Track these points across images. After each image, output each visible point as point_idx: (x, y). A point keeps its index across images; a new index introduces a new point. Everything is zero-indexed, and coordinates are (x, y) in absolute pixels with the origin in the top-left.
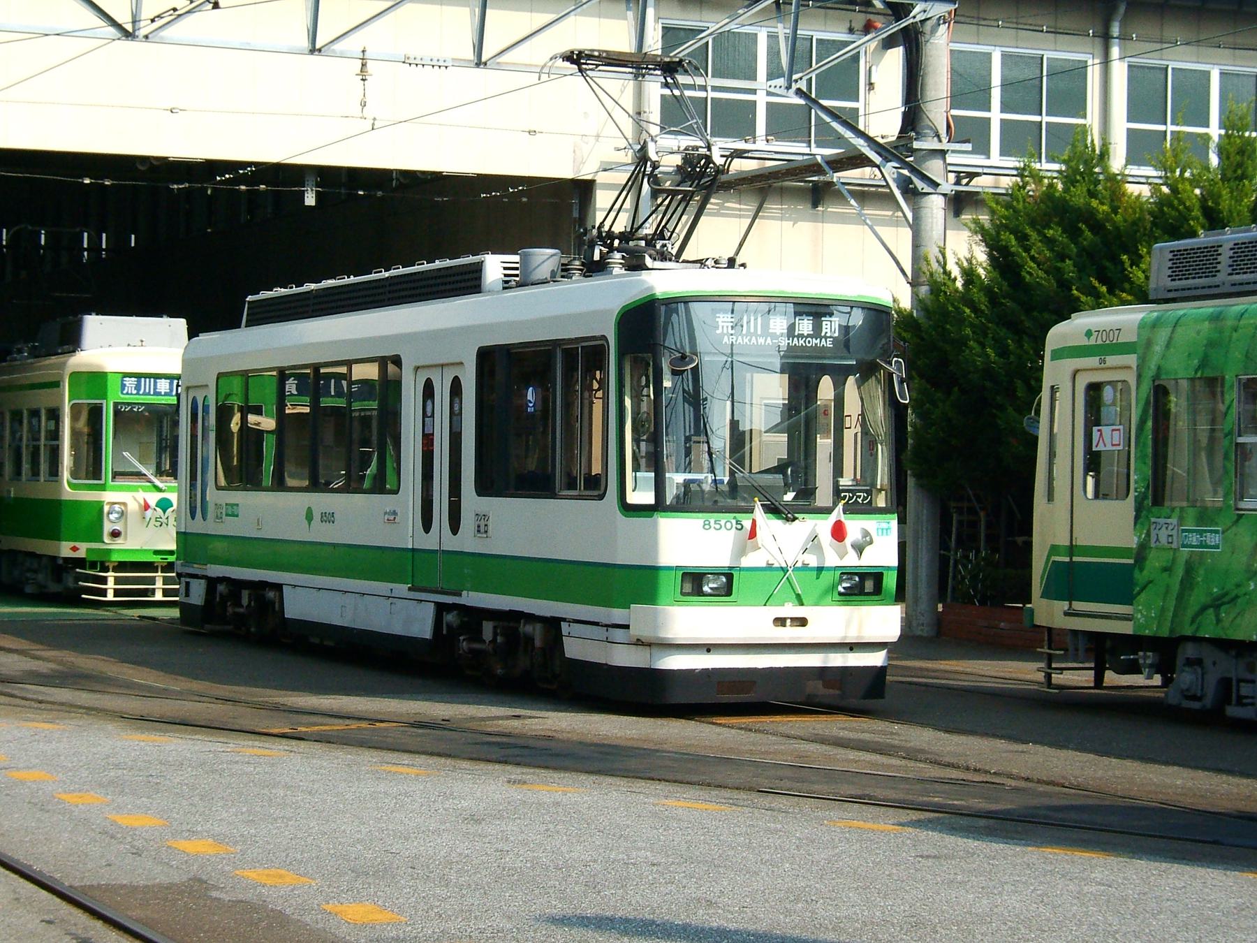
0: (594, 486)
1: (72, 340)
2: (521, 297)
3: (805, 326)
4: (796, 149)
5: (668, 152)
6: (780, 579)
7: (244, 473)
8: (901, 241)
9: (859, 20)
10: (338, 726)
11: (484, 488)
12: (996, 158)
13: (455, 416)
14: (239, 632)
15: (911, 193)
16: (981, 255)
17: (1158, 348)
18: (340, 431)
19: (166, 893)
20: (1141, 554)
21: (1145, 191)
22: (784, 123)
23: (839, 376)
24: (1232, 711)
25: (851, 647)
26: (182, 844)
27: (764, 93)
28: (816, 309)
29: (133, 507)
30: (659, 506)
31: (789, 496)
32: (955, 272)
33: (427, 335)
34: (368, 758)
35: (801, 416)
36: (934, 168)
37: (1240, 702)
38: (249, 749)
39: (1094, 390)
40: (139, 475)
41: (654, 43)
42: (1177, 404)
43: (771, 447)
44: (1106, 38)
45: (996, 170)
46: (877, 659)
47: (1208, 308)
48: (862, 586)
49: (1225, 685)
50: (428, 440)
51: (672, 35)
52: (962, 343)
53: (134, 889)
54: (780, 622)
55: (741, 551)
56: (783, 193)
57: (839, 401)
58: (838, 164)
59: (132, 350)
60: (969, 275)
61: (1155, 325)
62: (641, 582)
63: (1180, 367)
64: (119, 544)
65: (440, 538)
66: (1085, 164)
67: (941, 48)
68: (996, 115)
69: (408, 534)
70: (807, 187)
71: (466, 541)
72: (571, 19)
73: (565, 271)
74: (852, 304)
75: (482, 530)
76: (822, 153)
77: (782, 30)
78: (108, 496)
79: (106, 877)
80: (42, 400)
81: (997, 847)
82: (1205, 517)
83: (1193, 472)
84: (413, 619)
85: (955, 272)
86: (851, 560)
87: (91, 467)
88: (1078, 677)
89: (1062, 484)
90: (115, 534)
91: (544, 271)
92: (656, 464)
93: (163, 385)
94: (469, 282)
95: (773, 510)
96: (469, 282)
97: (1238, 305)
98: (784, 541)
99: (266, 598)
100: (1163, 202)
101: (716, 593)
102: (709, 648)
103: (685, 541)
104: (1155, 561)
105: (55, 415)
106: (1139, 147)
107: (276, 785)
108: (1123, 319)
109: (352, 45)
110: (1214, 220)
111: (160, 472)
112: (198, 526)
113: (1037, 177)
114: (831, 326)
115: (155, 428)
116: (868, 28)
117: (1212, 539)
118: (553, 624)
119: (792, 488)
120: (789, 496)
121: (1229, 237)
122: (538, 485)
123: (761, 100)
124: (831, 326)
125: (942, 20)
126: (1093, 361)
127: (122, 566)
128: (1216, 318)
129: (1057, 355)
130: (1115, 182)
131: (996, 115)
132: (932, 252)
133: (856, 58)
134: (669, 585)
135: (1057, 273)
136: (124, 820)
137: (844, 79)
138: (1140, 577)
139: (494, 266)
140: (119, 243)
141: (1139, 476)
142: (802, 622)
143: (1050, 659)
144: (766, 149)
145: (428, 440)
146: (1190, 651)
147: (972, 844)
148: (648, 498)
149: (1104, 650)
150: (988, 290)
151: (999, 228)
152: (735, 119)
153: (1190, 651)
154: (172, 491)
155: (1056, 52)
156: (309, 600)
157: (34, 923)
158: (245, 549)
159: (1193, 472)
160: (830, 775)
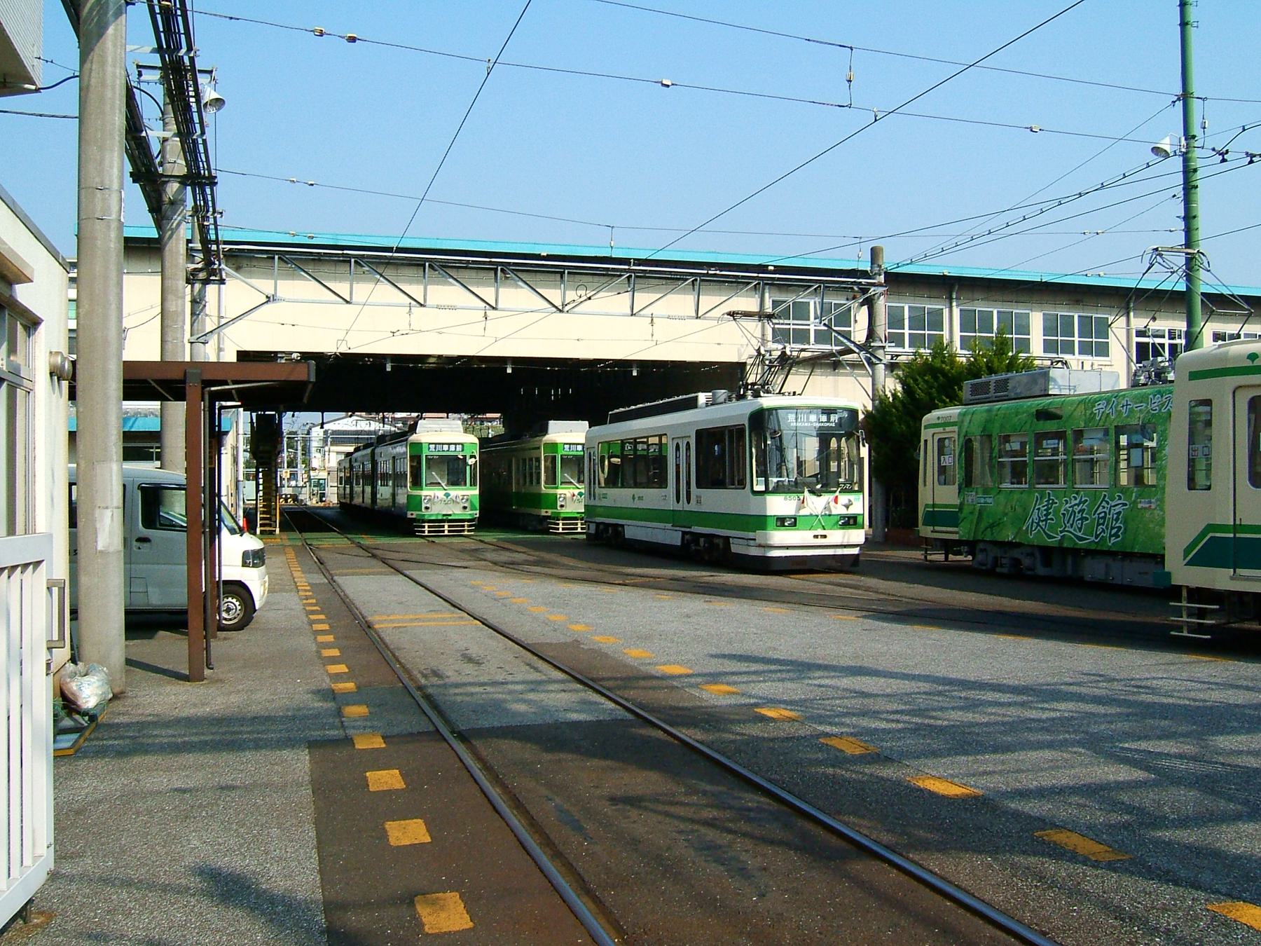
0: (741, 484)
1: (545, 431)
2: (711, 409)
3: (824, 418)
4: (826, 348)
5: (776, 349)
6: (817, 520)
7: (612, 482)
8: (867, 383)
9: (851, 295)
10: (639, 580)
11: (699, 486)
12: (907, 349)
13: (688, 457)
14: (608, 545)
15: (871, 364)
16: (899, 388)
17: (966, 424)
18: (640, 466)
19: (564, 645)
20: (961, 507)
21: (964, 360)
22: (821, 337)
23: (839, 437)
24: (998, 570)
25: (845, 546)
26: (573, 627)
27: (813, 326)
28: (828, 411)
29: (569, 495)
30: (767, 491)
31: (819, 486)
32: (889, 395)
33: (669, 428)
34: (652, 592)
35: (825, 454)
36: (880, 353)
37: (1002, 566)
38: (606, 589)
39: (941, 441)
40: (439, 484)
41: (768, 308)
42: (976, 445)
43: (812, 468)
44: (951, 299)
45: (905, 353)
46: (856, 551)
47: (986, 406)
48: (850, 522)
49: (996, 559)
50: (678, 466)
51: (775, 304)
52: (891, 423)
53: (551, 644)
54: (816, 537)
55: (799, 509)
56: (822, 365)
57: (839, 446)
58: (842, 353)
59: (568, 434)
60: (894, 395)
61: (964, 414)
62: (760, 522)
63: (976, 431)
64: (564, 510)
65: (683, 506)
66: (939, 348)
67: (882, 305)
68: (907, 331)
69: (671, 505)
70: (829, 363)
71: (693, 507)
72: (669, 296)
73: (730, 399)
74: (845, 409)
75: (699, 502)
76: (835, 348)
77: (818, 300)
78: (559, 491)
79: (542, 640)
80: (534, 454)
81: (894, 625)
82: (986, 491)
83: (983, 473)
84: (675, 538)
85: (889, 395)
86: (844, 511)
87: (552, 480)
88: (939, 557)
89: (929, 480)
90: (427, 508)
91: (721, 399)
92: (763, 473)
93: (446, 447)
94: (692, 404)
95: (812, 492)
96: (692, 404)
97: (998, 405)
98: (816, 504)
99: (618, 530)
100: (971, 364)
101: (790, 525)
102: (787, 548)
103: (778, 505)
104: (966, 510)
105: (538, 460)
106: (965, 342)
107: (612, 603)
108: (953, 412)
109: (647, 312)
110: (991, 370)
111: (579, 482)
112: (592, 503)
113: (921, 356)
114: (834, 418)
115: (575, 464)
116: (854, 298)
117: (989, 500)
118: (727, 538)
119: (825, 482)
120: (819, 486)
121: (994, 377)
122: (718, 484)
123: (812, 328)
124: (834, 418)
125: (881, 294)
126: (941, 429)
127: (565, 519)
128: (989, 411)
129: (926, 427)
130: (953, 356)
131: (907, 331)
132: (880, 387)
133: (849, 309)
134: (771, 523)
135: (929, 394)
136: (552, 618)
137: (845, 318)
138: (962, 516)
139: (702, 397)
140: (565, 393)
141: (959, 475)
142: (825, 536)
143: (926, 550)
144: (814, 348)
145: (678, 466)
146: (981, 546)
147: (885, 624)
148: (762, 488)
149: (948, 546)
150: (902, 402)
151: (906, 377)
152: (802, 336)
153: (981, 546)
154: (582, 488)
155: (930, 305)
156: (634, 531)
157: (511, 658)
158: (611, 511)
159: (983, 473)
160: (832, 598)
